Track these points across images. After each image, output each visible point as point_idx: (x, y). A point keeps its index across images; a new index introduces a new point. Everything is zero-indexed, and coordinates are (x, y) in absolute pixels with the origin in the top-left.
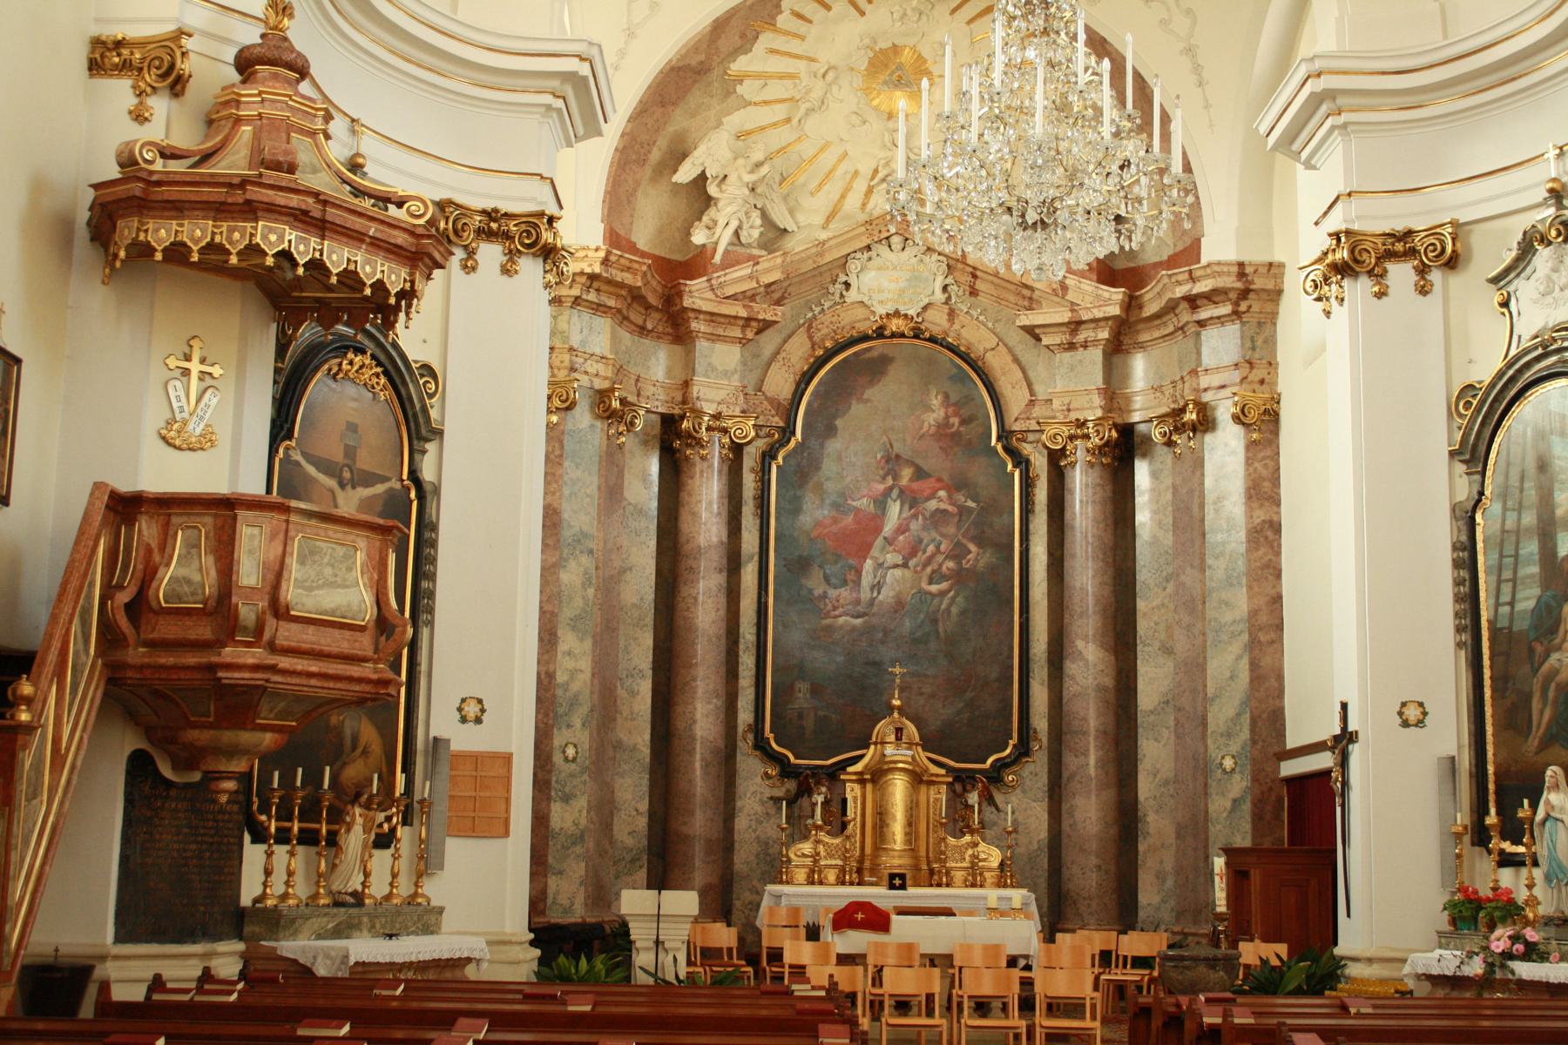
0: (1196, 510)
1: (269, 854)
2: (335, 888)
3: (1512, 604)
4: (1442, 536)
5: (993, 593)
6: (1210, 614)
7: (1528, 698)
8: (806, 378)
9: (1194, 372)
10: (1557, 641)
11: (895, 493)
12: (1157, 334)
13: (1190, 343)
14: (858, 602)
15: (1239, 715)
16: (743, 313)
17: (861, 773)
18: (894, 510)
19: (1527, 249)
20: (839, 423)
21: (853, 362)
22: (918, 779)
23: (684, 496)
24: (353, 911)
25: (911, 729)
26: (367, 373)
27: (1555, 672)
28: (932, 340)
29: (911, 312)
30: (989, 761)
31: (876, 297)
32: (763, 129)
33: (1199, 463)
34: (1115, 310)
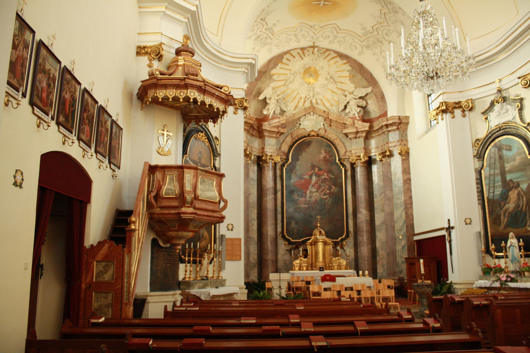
0: (389, 176)
1: (186, 266)
2: (201, 275)
3: (493, 193)
4: (473, 176)
5: (338, 198)
6: (394, 201)
7: (500, 216)
8: (291, 147)
9: (388, 143)
10: (508, 201)
11: (314, 174)
12: (377, 134)
13: (386, 136)
14: (306, 201)
15: (403, 225)
16: (277, 131)
17: (311, 243)
18: (314, 179)
19: (492, 104)
20: (300, 157)
21: (302, 143)
22: (325, 243)
23: (263, 176)
24: (207, 281)
25: (323, 232)
26: (204, 138)
27: (507, 209)
28: (321, 137)
29: (316, 130)
30: (339, 239)
31: (307, 127)
32: (279, 87)
33: (389, 165)
34: (367, 129)
